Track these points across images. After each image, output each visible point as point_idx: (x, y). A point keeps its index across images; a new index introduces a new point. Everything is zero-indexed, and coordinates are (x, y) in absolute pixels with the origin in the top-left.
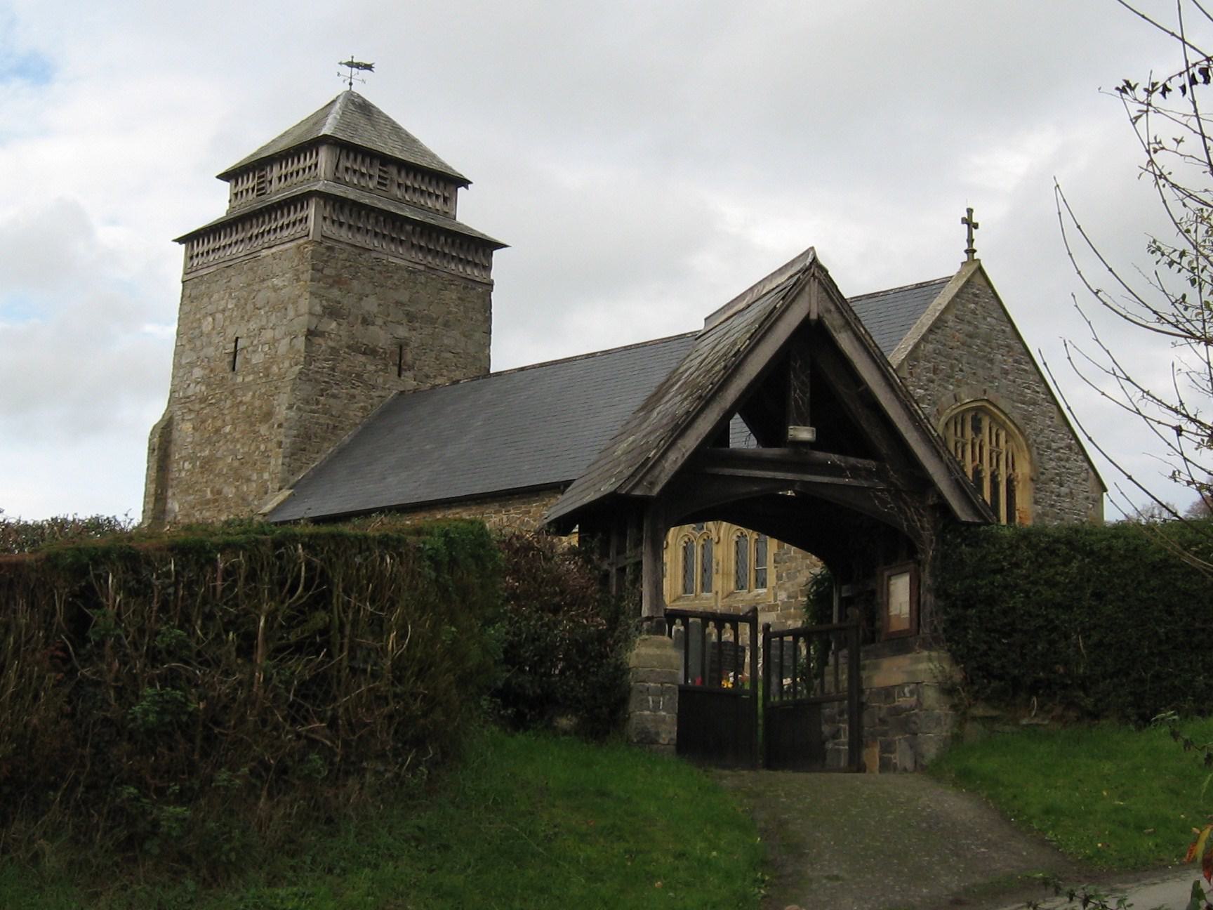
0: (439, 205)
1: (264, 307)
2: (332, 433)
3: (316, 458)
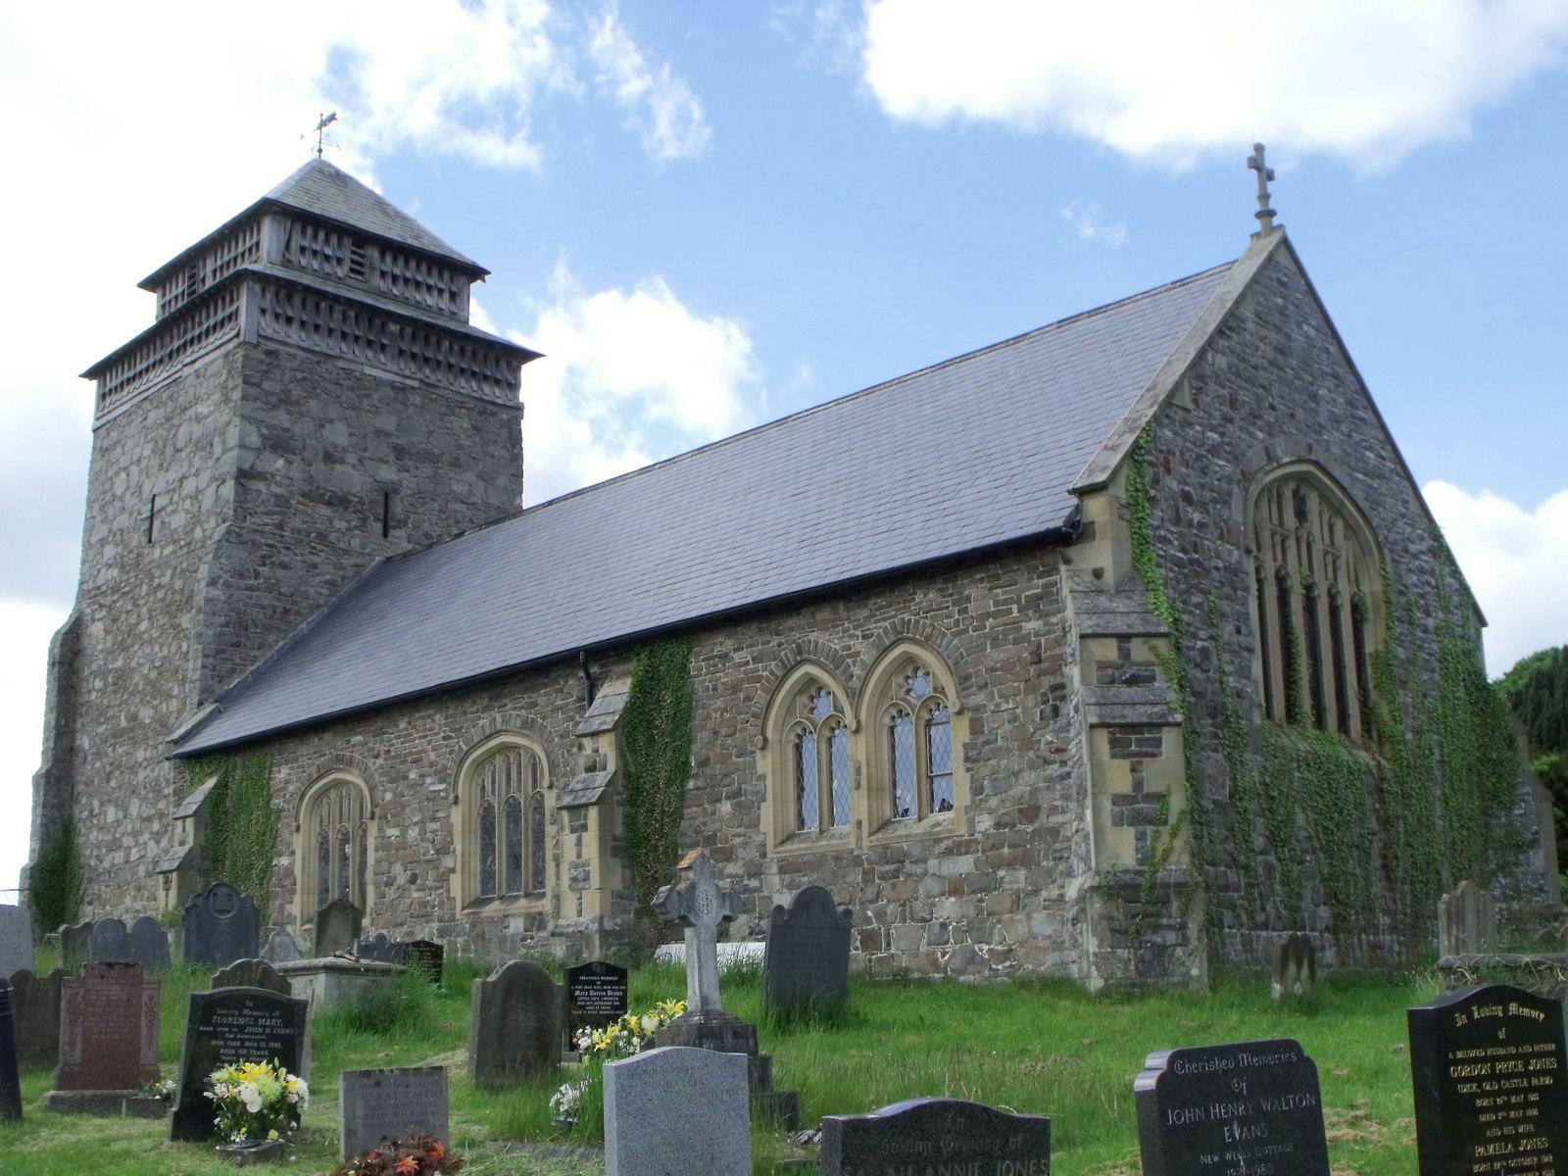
0: (444, 303)
1: (186, 447)
2: (281, 620)
3: (257, 657)
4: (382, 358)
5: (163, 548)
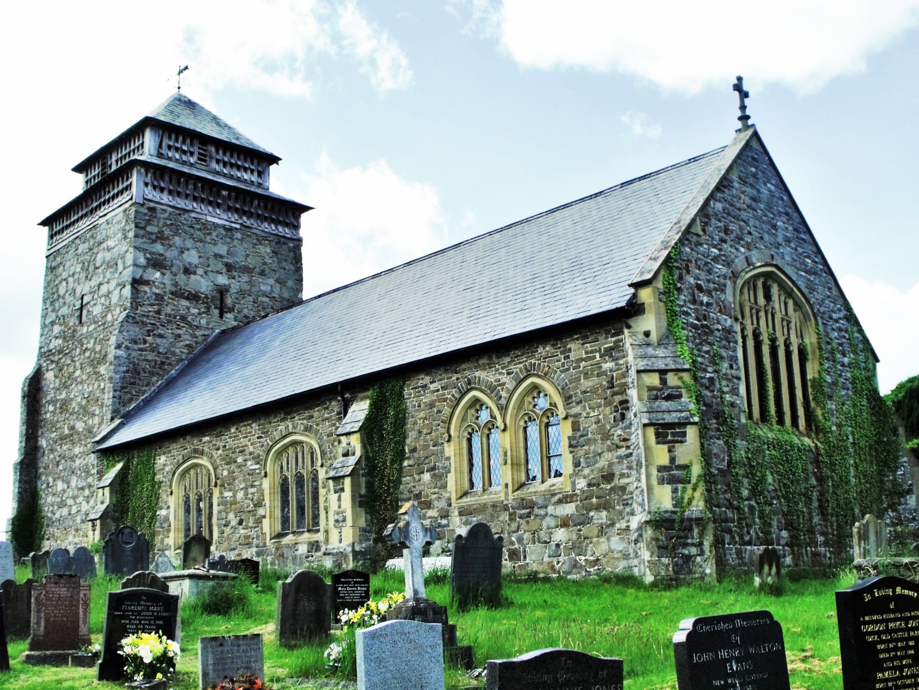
1: (101, 266)
2: (160, 368)
3: (145, 391)
4: (218, 211)
5: (88, 326)
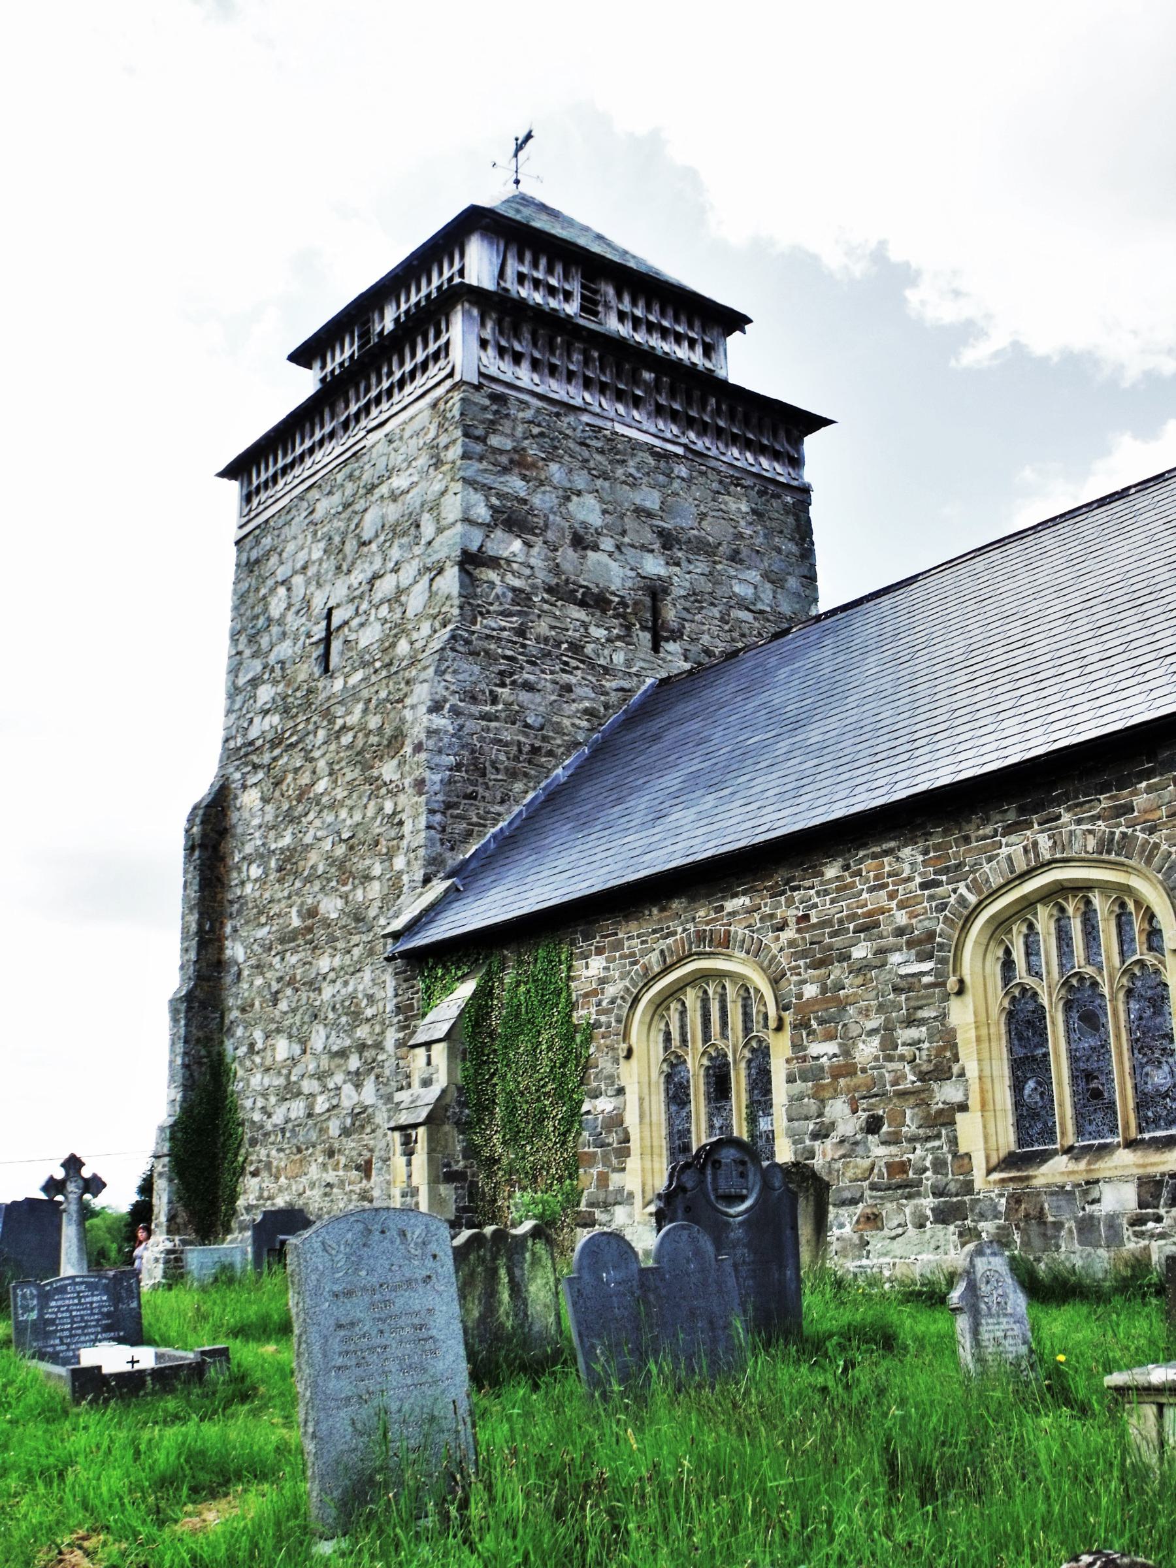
1: (377, 536)
2: (530, 762)
3: (499, 814)
4: (635, 413)
5: (347, 676)
